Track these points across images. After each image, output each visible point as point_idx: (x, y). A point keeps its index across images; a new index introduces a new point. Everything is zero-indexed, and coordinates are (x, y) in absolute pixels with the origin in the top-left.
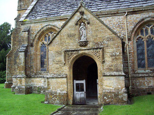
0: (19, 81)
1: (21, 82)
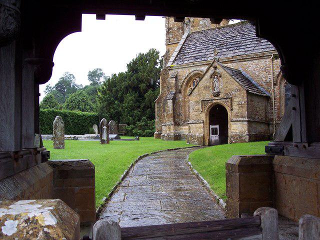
0: (168, 129)
1: (169, 129)
